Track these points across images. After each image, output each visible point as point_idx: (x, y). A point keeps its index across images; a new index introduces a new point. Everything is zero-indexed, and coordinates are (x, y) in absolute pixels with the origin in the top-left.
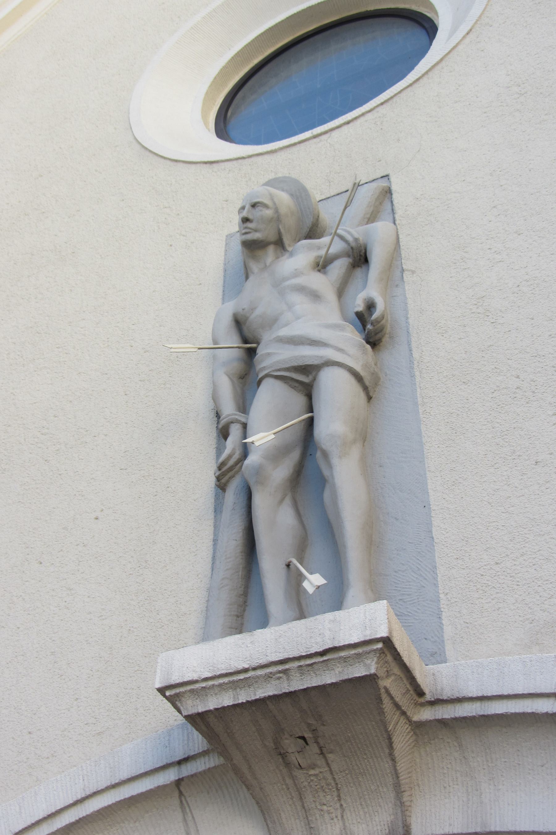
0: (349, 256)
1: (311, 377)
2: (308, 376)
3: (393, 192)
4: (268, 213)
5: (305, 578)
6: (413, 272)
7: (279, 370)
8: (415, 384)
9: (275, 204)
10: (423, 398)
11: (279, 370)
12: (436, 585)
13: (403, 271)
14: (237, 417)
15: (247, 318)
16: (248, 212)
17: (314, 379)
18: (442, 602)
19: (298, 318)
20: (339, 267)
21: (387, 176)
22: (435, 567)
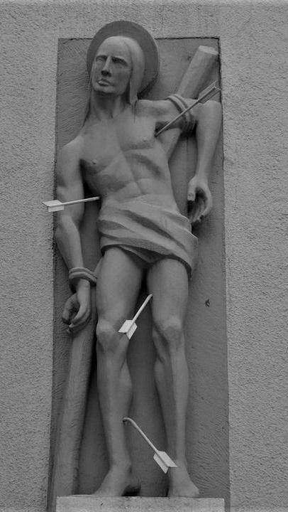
0: (181, 128)
1: (152, 261)
2: (150, 258)
3: (222, 63)
4: (126, 70)
5: (154, 452)
6: (232, 164)
7: (129, 246)
8: (225, 280)
9: (132, 63)
10: (230, 295)
11: (129, 246)
12: (227, 461)
13: (223, 159)
14: (86, 274)
15: (95, 172)
16: (109, 66)
17: (156, 263)
18: (231, 476)
19: (143, 193)
20: (172, 136)
21: (218, 39)
22: (228, 447)
